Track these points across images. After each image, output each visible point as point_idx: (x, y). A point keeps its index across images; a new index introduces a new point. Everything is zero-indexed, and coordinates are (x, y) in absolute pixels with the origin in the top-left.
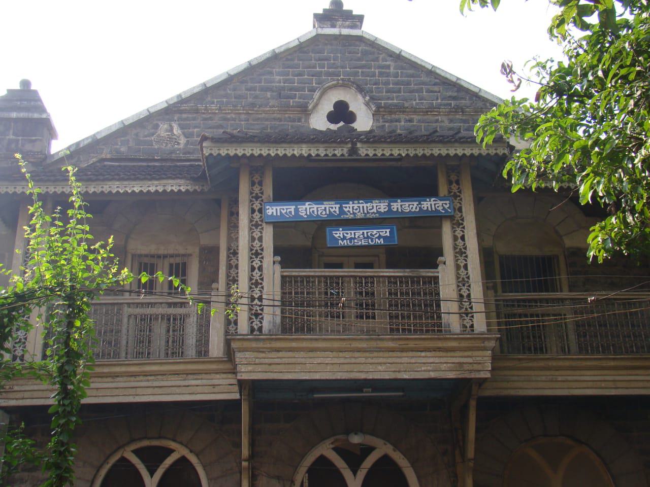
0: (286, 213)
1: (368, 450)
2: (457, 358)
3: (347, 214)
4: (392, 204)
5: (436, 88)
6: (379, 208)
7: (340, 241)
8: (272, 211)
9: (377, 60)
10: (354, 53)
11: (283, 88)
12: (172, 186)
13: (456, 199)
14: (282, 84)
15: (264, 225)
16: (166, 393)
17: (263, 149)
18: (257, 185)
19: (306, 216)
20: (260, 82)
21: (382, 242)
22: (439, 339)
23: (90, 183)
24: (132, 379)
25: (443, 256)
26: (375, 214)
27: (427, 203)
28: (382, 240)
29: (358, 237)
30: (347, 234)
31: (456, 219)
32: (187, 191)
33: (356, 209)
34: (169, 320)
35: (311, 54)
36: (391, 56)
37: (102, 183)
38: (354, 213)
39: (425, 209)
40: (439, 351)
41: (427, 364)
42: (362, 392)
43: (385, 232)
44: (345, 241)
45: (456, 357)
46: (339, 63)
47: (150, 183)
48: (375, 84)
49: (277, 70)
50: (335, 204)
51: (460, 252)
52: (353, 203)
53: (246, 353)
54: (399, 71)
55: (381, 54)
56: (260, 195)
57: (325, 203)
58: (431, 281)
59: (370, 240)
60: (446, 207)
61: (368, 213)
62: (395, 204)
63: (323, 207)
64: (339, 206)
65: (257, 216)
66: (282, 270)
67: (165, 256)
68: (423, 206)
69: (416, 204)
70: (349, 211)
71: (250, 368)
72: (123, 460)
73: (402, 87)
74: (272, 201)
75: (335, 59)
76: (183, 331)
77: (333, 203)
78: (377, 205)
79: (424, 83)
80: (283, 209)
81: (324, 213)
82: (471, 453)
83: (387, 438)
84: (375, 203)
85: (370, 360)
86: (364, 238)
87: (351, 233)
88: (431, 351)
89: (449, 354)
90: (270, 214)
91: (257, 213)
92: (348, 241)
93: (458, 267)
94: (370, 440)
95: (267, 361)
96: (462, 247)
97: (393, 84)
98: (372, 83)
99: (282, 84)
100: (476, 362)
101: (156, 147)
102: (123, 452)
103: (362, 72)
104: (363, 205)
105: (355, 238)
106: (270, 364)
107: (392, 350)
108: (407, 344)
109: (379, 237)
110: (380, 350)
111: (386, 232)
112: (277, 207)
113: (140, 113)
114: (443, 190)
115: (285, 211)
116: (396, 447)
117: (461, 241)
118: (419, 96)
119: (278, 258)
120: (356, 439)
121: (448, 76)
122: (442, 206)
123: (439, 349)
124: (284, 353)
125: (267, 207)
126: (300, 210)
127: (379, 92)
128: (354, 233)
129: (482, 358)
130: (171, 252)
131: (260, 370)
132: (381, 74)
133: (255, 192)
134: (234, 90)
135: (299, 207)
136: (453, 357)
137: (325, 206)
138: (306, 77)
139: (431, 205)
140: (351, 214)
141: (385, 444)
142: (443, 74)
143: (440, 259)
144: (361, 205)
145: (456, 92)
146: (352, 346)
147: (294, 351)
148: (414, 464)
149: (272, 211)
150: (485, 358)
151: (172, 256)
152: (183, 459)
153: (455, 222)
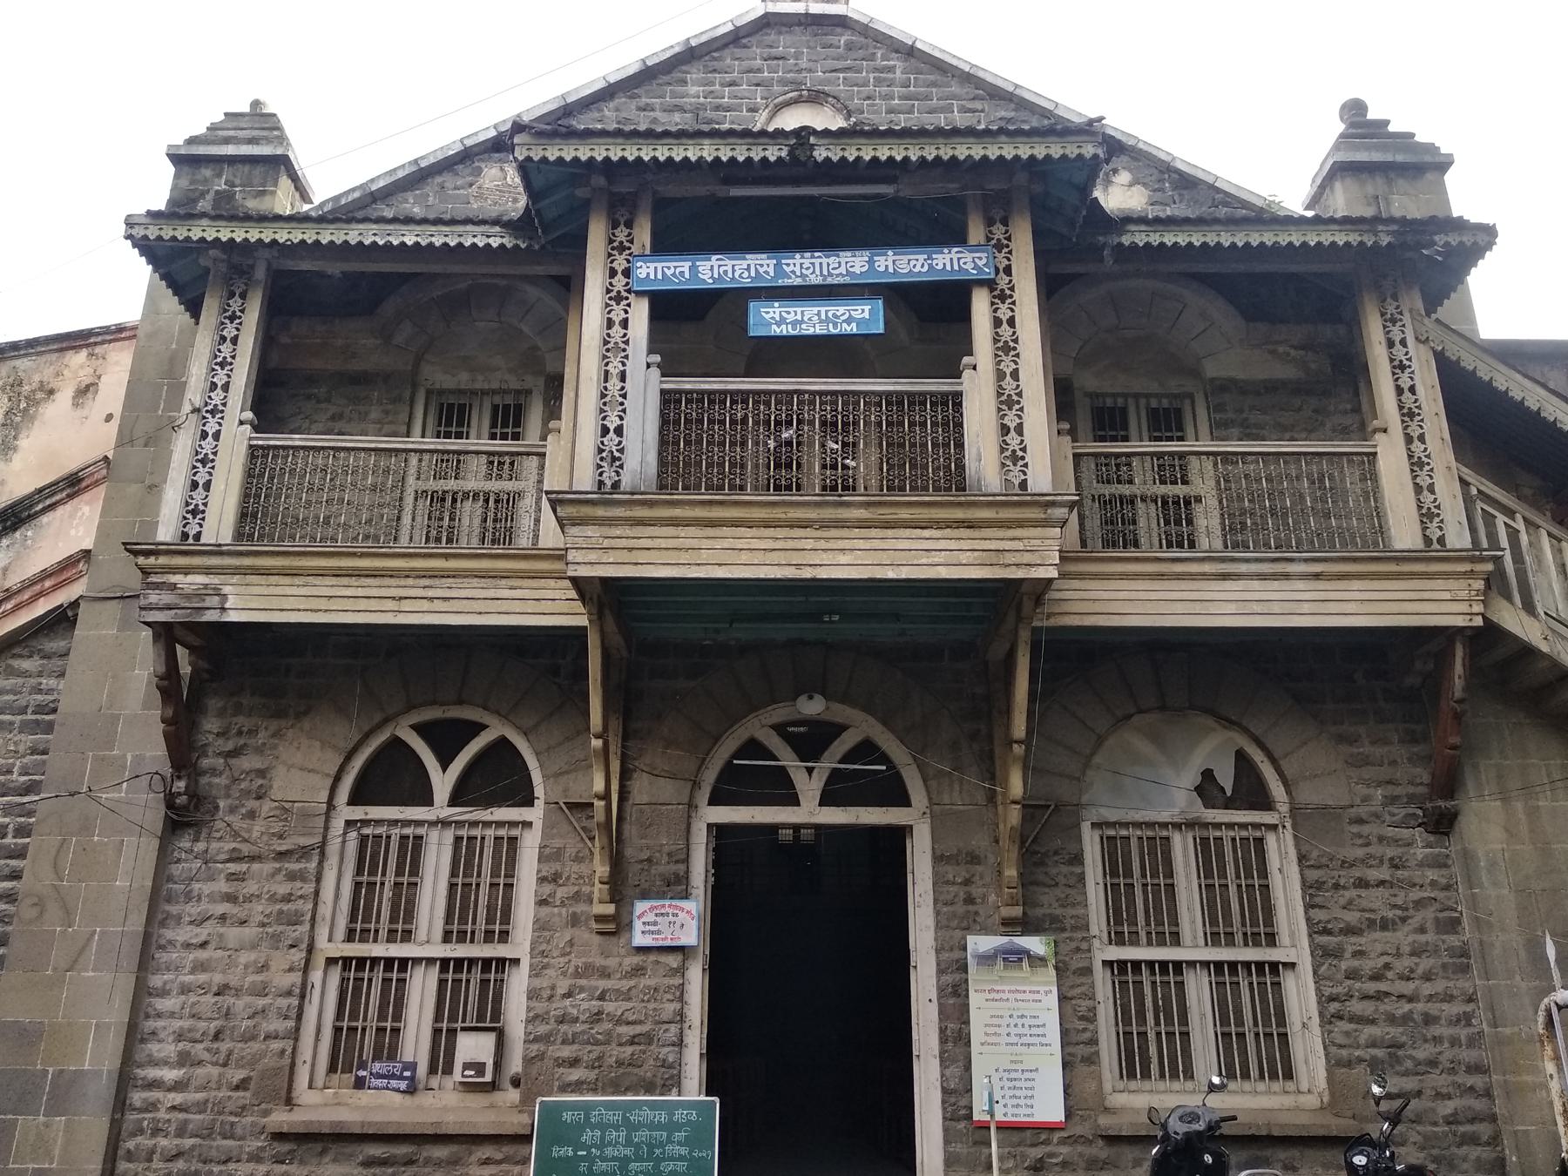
0: (674, 275)
3: (791, 278)
4: (876, 258)
5: (978, 105)
6: (852, 267)
7: (774, 327)
8: (648, 270)
9: (872, 57)
10: (831, 46)
11: (703, 107)
12: (474, 236)
13: (1000, 252)
14: (702, 99)
15: (632, 297)
16: (455, 610)
17: (628, 147)
18: (622, 227)
19: (711, 281)
20: (663, 97)
21: (855, 330)
22: (960, 504)
23: (324, 226)
25: (972, 355)
26: (843, 276)
27: (944, 256)
28: (854, 325)
29: (811, 319)
30: (789, 313)
31: (1000, 287)
32: (502, 246)
33: (808, 268)
34: (487, 501)
35: (754, 48)
36: (897, 51)
37: (345, 226)
38: (803, 276)
39: (940, 267)
43: (860, 311)
44: (784, 326)
46: (804, 63)
47: (433, 228)
48: (869, 98)
49: (694, 76)
50: (768, 258)
51: (1006, 348)
52: (802, 257)
54: (912, 77)
55: (879, 48)
56: (627, 244)
57: (748, 256)
58: (948, 400)
59: (831, 325)
60: (980, 263)
61: (830, 274)
62: (882, 258)
63: (744, 264)
64: (775, 262)
65: (619, 282)
66: (663, 379)
67: (484, 393)
68: (935, 262)
69: (922, 257)
70: (793, 272)
71: (592, 556)
72: (396, 743)
73: (916, 103)
74: (648, 252)
75: (797, 56)
76: (512, 520)
77: (764, 256)
78: (848, 260)
79: (954, 97)
80: (669, 268)
81: (746, 274)
82: (1019, 728)
83: (868, 709)
84: (846, 257)
85: (822, 544)
86: (821, 321)
87: (795, 312)
90: (643, 276)
91: (620, 276)
92: (790, 326)
93: (1000, 375)
94: (842, 713)
96: (1009, 339)
97: (900, 98)
98: (864, 95)
99: (702, 99)
100: (1029, 548)
101: (475, 206)
103: (844, 78)
104: (819, 260)
105: (802, 321)
108: (896, 514)
109: (849, 321)
111: (863, 311)
112: (656, 264)
113: (448, 147)
114: (976, 233)
115: (672, 270)
117: (1008, 328)
118: (945, 117)
119: (657, 358)
120: (812, 707)
121: (1000, 83)
122: (974, 261)
125: (639, 264)
126: (700, 269)
127: (874, 112)
128: (802, 312)
130: (495, 385)
131: (611, 560)
132: (878, 82)
133: (619, 239)
134: (617, 110)
135: (698, 263)
137: (748, 262)
138: (744, 87)
139: (951, 259)
140: (797, 277)
142: (989, 79)
143: (966, 360)
144: (817, 261)
145: (1013, 110)
146: (789, 515)
147: (678, 525)
149: (648, 270)
150: (1048, 542)
151: (494, 392)
152: (503, 743)
153: (996, 293)
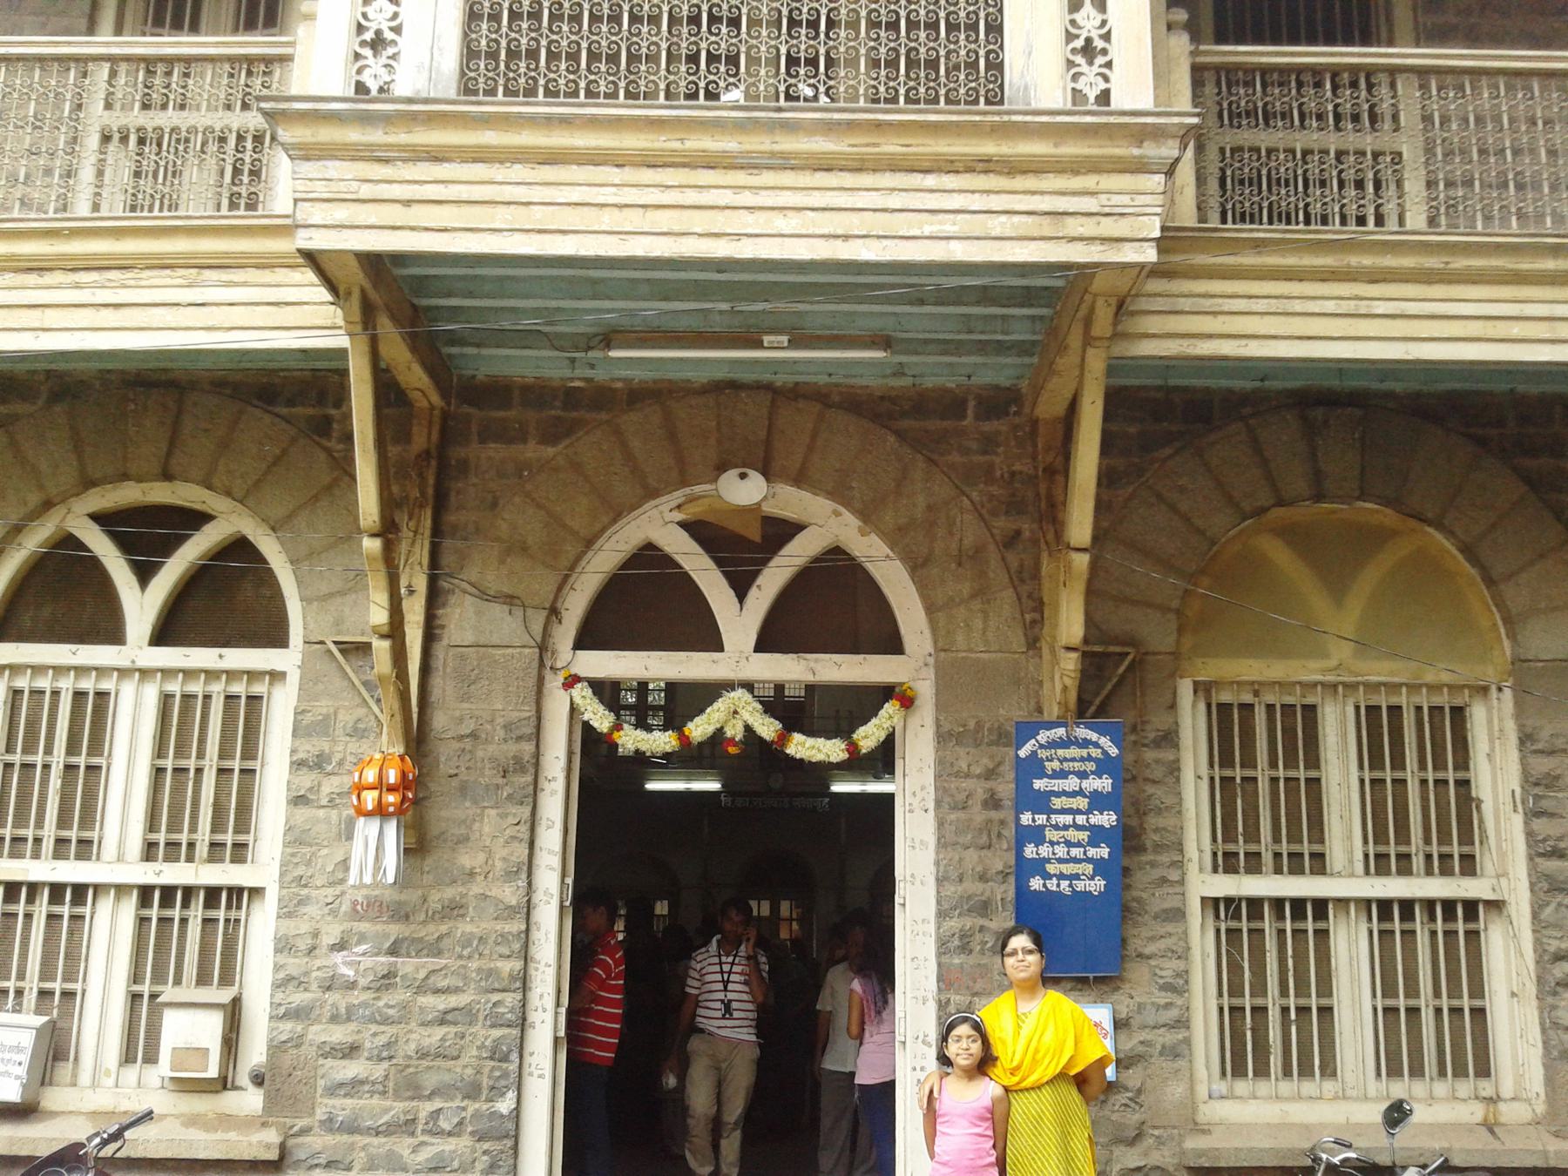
1: (780, 532)
2: (1047, 198)
24: (32, 279)
40: (986, 172)
41: (941, 216)
42: (759, 345)
45: (1042, 193)
53: (330, 163)
83: (839, 494)
88: (957, 172)
89: (1020, 182)
94: (791, 501)
95: (397, 191)
100: (1107, 210)
102: (64, 518)
106: (408, 203)
107: (825, 165)
108: (874, 145)
110: (785, 162)
116: (868, 516)
123: (986, 165)
124: (454, 165)
129: (1132, 200)
136: (1034, 193)
141: (837, 514)
148: (917, 566)
150: (1141, 200)
